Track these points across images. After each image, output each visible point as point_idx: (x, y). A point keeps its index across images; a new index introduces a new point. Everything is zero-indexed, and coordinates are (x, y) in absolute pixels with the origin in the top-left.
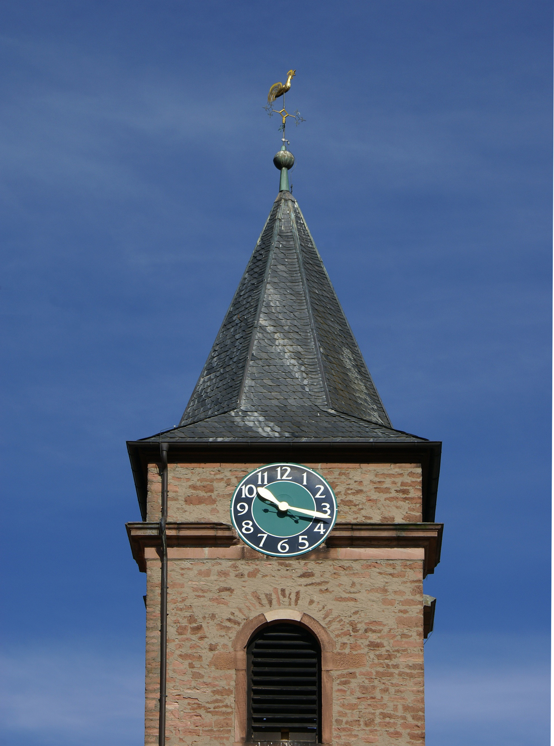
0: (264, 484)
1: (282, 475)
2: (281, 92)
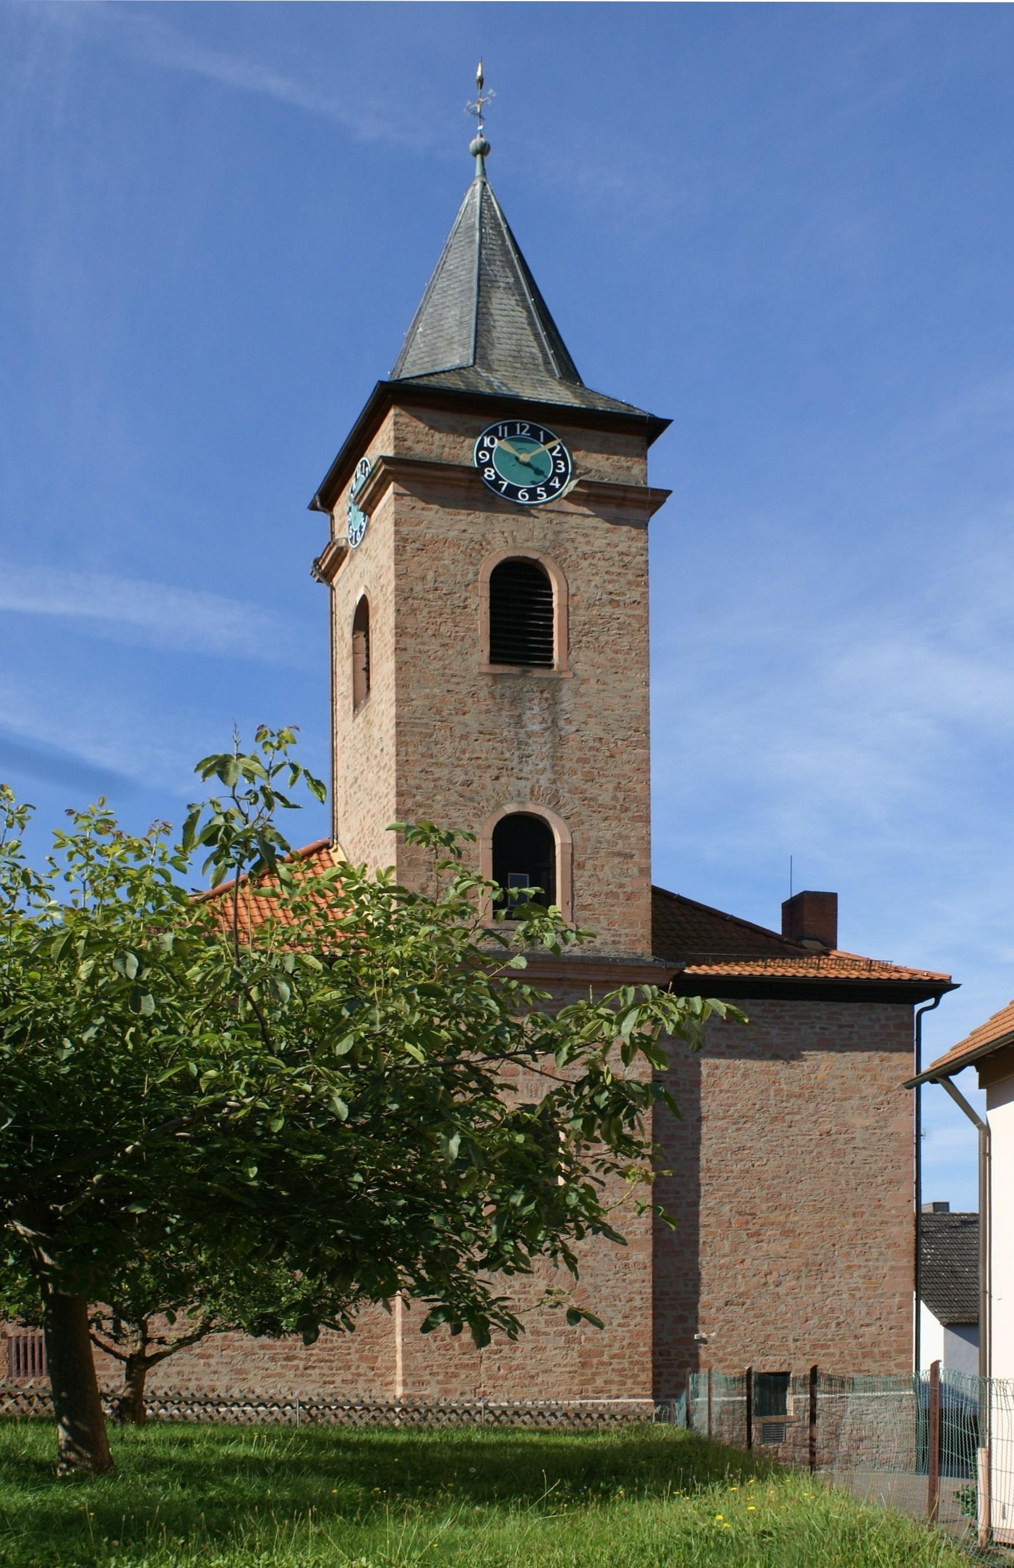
0: (951, 1078)
1: (521, 431)
2: (481, 81)
